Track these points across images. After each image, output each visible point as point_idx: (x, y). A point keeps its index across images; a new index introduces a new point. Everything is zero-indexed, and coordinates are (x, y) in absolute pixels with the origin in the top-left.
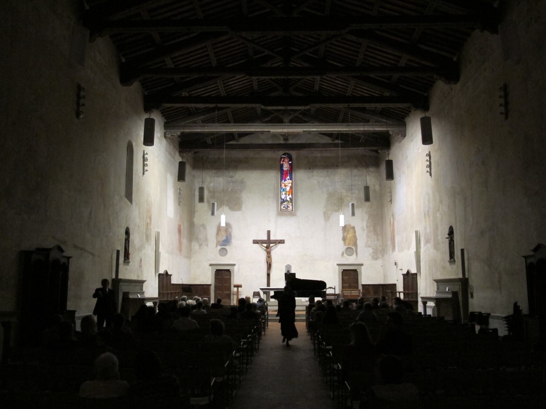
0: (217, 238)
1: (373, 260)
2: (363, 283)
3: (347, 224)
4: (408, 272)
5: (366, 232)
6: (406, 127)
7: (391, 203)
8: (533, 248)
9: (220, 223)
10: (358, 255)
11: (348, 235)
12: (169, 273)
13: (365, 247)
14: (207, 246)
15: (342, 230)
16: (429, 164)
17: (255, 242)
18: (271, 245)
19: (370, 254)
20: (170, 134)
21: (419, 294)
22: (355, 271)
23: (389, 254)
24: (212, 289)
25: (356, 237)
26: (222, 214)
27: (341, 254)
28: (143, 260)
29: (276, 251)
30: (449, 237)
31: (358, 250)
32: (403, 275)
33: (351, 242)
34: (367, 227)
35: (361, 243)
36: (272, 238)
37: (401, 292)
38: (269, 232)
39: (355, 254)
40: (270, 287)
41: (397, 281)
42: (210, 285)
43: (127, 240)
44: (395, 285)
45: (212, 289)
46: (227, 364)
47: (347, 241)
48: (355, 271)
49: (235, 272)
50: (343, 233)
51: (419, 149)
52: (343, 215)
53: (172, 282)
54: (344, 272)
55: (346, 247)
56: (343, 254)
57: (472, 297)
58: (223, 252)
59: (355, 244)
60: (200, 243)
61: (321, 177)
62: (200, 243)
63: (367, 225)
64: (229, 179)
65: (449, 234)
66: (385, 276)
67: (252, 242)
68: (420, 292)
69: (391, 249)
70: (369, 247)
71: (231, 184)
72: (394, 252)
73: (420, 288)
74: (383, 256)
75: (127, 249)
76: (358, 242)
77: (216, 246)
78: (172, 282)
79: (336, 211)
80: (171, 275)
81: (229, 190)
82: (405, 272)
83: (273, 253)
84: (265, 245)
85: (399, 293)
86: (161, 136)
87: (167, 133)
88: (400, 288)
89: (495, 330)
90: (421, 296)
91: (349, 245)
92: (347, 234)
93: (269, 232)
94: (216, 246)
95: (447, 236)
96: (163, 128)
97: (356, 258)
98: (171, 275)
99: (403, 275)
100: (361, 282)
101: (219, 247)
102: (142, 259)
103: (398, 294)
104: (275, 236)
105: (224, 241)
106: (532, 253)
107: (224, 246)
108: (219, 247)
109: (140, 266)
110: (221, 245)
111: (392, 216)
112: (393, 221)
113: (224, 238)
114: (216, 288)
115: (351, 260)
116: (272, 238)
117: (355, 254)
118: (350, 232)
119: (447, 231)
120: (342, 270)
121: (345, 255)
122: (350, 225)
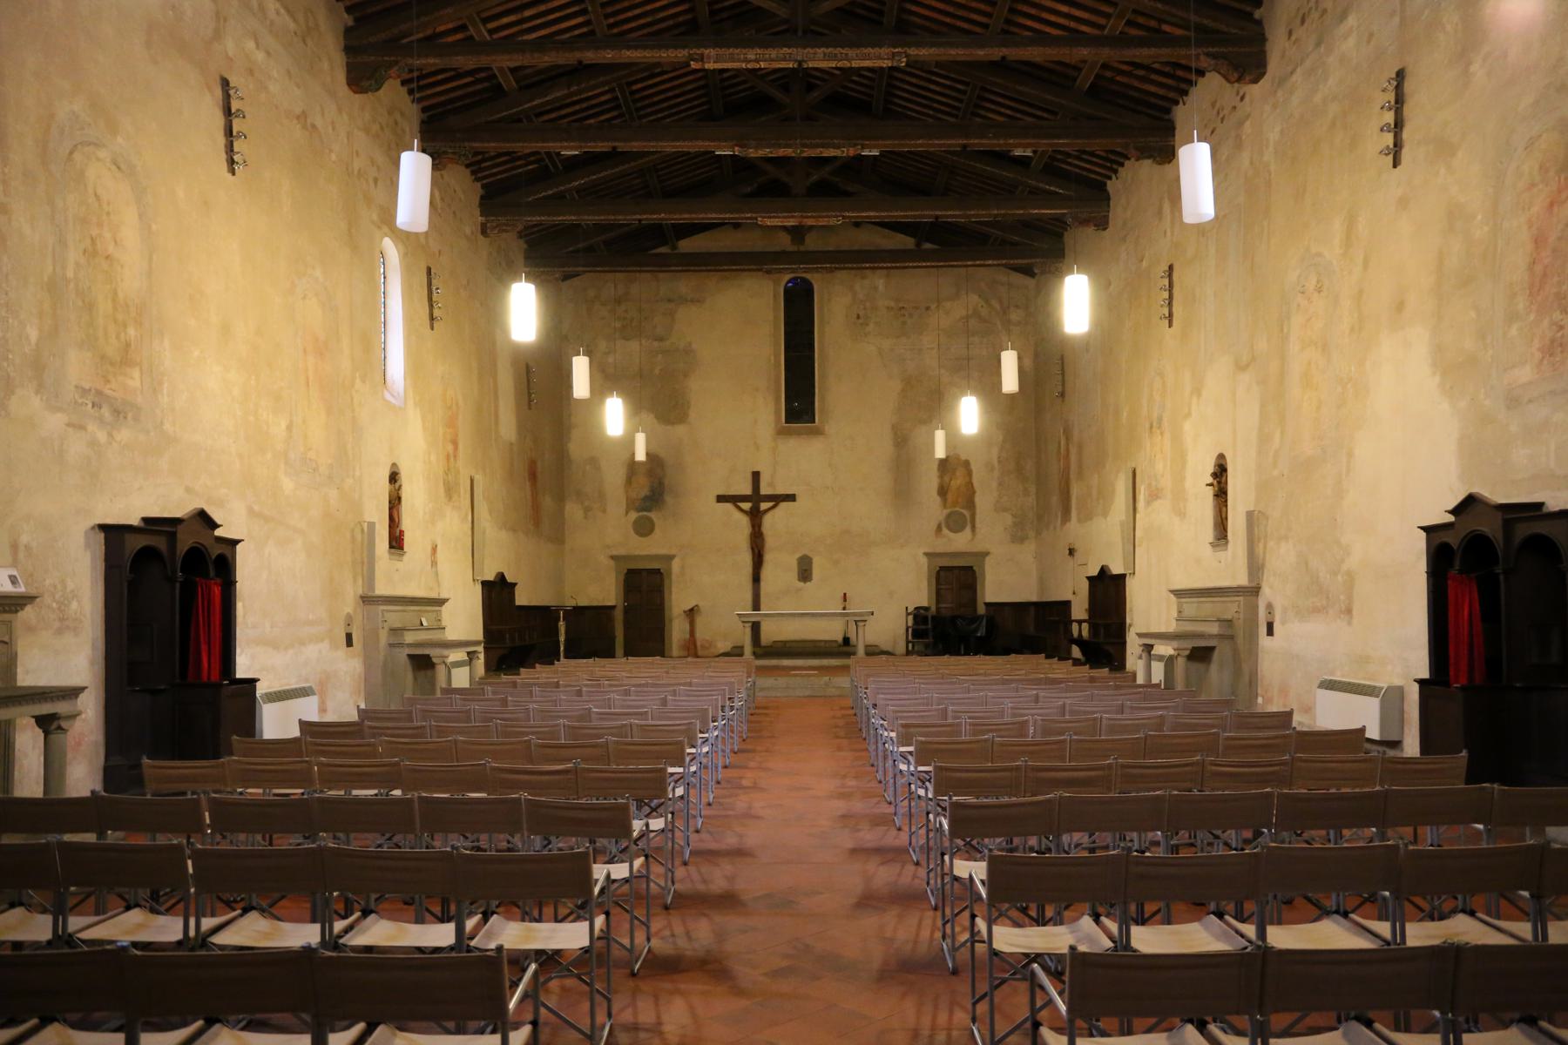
0: (627, 492)
1: (1013, 542)
2: (988, 600)
3: (952, 454)
4: (1103, 570)
5: (996, 473)
6: (1109, 206)
7: (1063, 401)
8: (1452, 505)
9: (634, 454)
10: (977, 530)
11: (952, 482)
12: (509, 579)
13: (995, 510)
14: (604, 511)
15: (939, 470)
16: (1167, 297)
17: (721, 499)
18: (764, 506)
19: (1006, 529)
20: (496, 227)
21: (1130, 626)
22: (969, 570)
23: (1055, 528)
24: (619, 616)
25: (972, 484)
26: (578, 354)
27: (935, 528)
28: (438, 547)
29: (775, 521)
30: (1215, 483)
31: (977, 520)
32: (1090, 579)
33: (960, 500)
34: (999, 462)
35: (984, 502)
36: (765, 490)
37: (1085, 621)
38: (756, 476)
39: (968, 529)
40: (759, 610)
41: (1074, 593)
42: (613, 607)
43: (395, 502)
44: (1066, 605)
45: (619, 616)
46: (1046, 212)
47: (950, 497)
48: (969, 570)
49: (674, 577)
50: (941, 477)
51: (1142, 261)
52: (943, 431)
53: (518, 603)
54: (942, 573)
55: (948, 511)
56: (939, 528)
57: (1270, 632)
58: (644, 528)
59: (971, 505)
60: (586, 504)
61: (888, 338)
62: (586, 504)
63: (999, 457)
64: (656, 344)
65: (1215, 475)
66: (1042, 583)
67: (715, 499)
68: (1132, 619)
69: (1059, 514)
70: (1005, 510)
71: (660, 356)
72: (1068, 524)
73: (1131, 610)
74: (1038, 533)
75: (397, 520)
76: (978, 499)
77: (627, 513)
78: (518, 603)
79: (924, 422)
80: (514, 585)
81: (657, 371)
82: (1094, 572)
83: (769, 522)
84: (746, 506)
85: (1080, 622)
86: (472, 233)
87: (488, 225)
88: (1079, 610)
89: (1134, 675)
90: (1138, 631)
91: (955, 507)
92: (951, 480)
93: (756, 476)
94: (627, 513)
95: (1210, 480)
96: (478, 212)
97: (973, 539)
98: (514, 585)
99: (1090, 579)
100: (983, 595)
101: (634, 515)
102: (436, 546)
103: (1075, 627)
104: (771, 485)
105: (646, 498)
106: (1451, 518)
107: (646, 510)
108: (634, 515)
109: (432, 562)
110: (639, 510)
111: (1064, 431)
112: (1068, 445)
113: (645, 492)
114: (626, 611)
115: (960, 542)
116: (765, 490)
117: (968, 529)
118: (958, 474)
119: (1210, 468)
120: (938, 569)
121: (945, 531)
122: (958, 458)
